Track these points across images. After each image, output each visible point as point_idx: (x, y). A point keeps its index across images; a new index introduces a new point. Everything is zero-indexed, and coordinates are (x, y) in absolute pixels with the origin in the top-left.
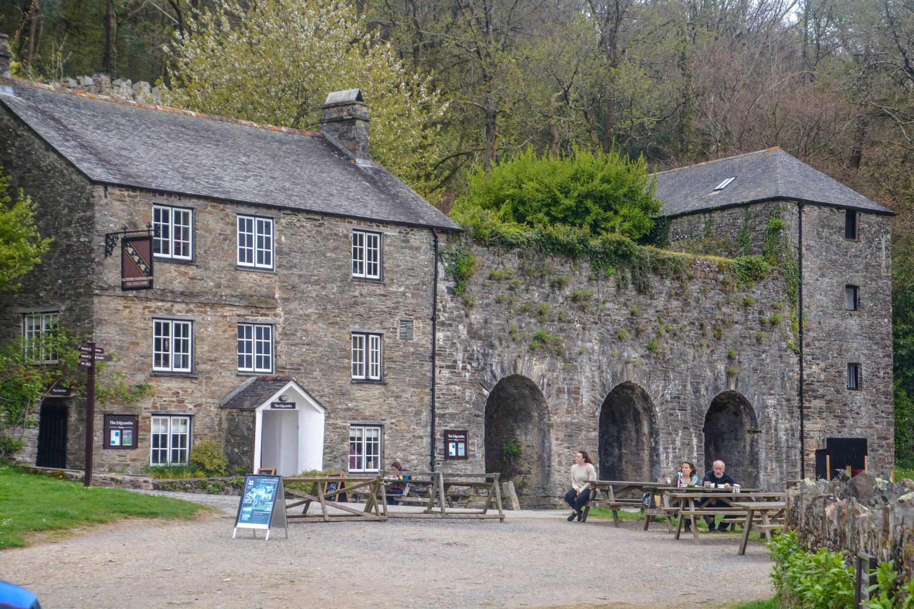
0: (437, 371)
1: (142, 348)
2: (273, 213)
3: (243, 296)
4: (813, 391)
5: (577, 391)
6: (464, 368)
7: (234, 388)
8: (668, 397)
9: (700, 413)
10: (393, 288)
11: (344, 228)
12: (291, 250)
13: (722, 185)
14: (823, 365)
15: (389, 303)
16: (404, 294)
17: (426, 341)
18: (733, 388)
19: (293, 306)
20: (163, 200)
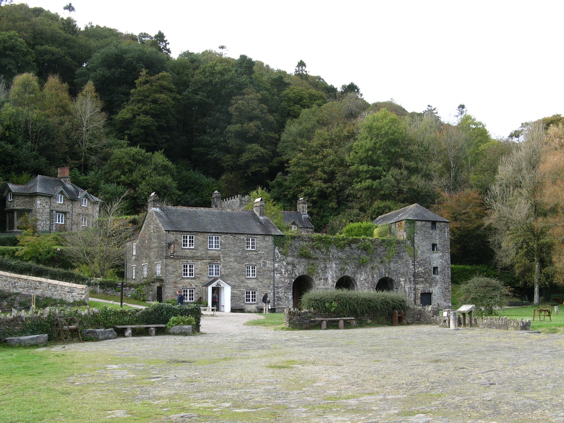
0: (275, 275)
1: (179, 271)
2: (220, 234)
3: (209, 257)
4: (420, 276)
5: (327, 279)
6: (285, 274)
7: (207, 281)
8: (362, 279)
9: (375, 284)
10: (260, 252)
11: (242, 237)
12: (225, 244)
13: (145, 269)
14: (423, 268)
15: (258, 256)
16: (263, 254)
17: (272, 266)
18: (387, 276)
19: (226, 258)
20: (185, 233)
